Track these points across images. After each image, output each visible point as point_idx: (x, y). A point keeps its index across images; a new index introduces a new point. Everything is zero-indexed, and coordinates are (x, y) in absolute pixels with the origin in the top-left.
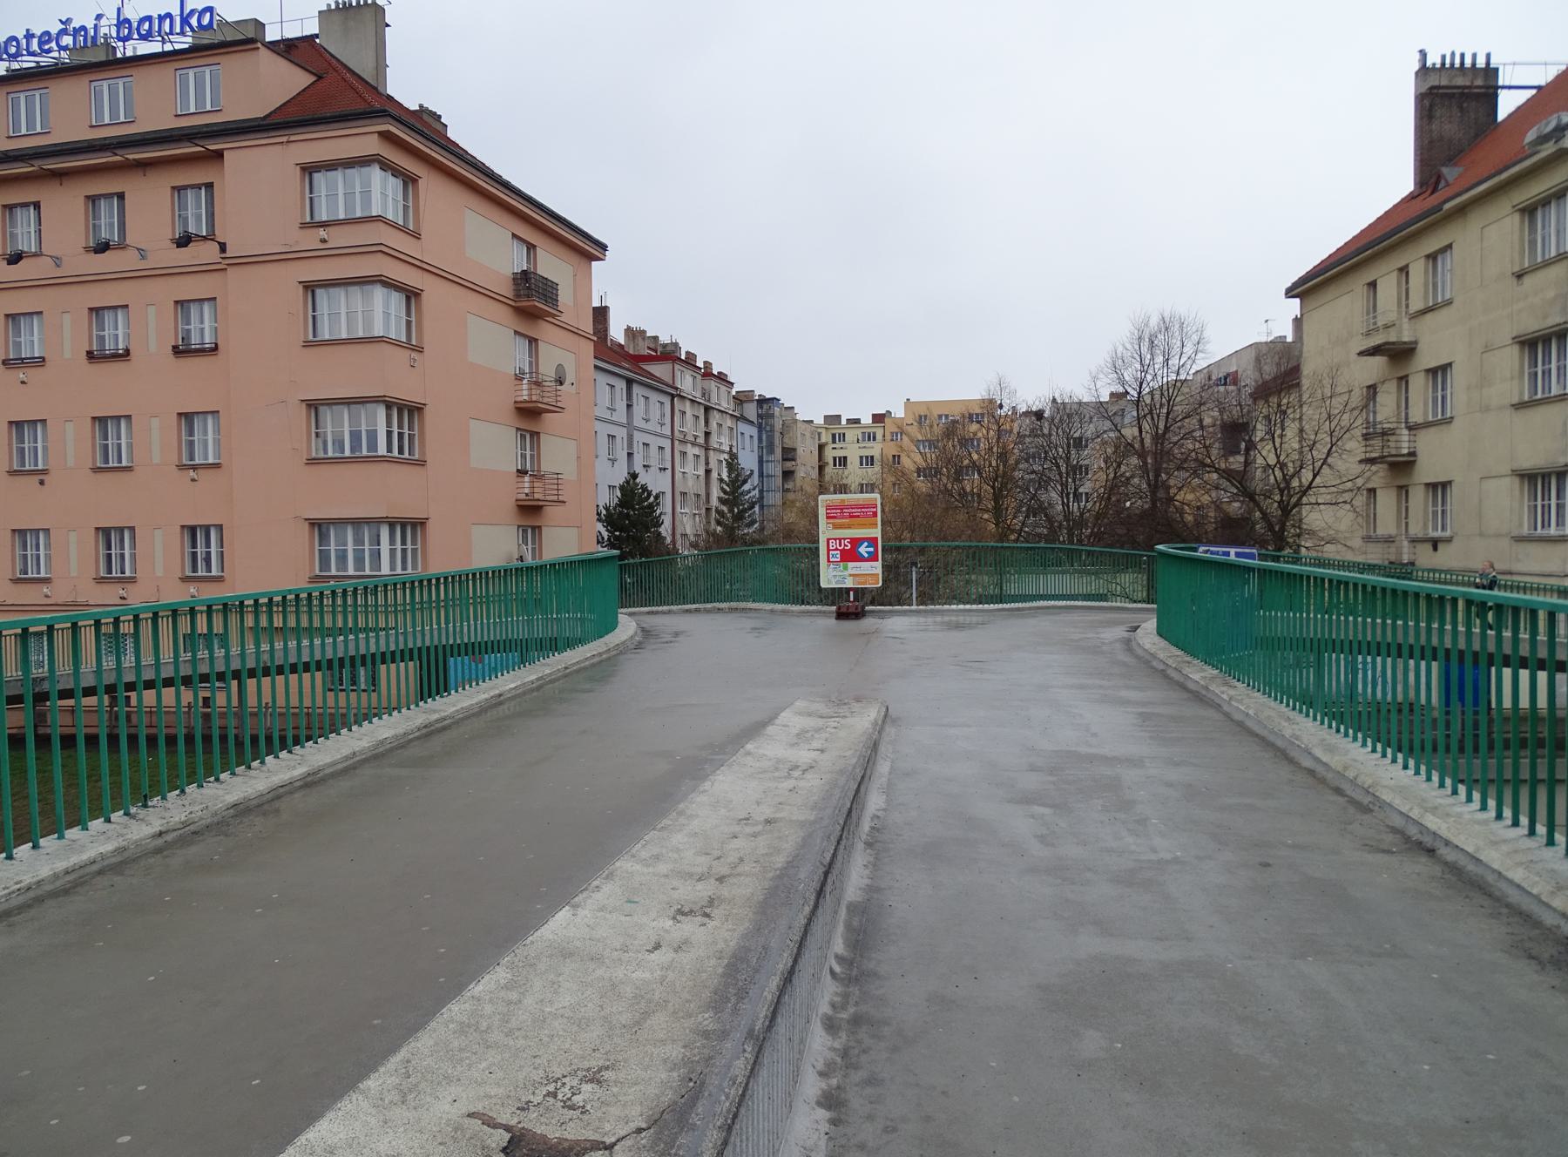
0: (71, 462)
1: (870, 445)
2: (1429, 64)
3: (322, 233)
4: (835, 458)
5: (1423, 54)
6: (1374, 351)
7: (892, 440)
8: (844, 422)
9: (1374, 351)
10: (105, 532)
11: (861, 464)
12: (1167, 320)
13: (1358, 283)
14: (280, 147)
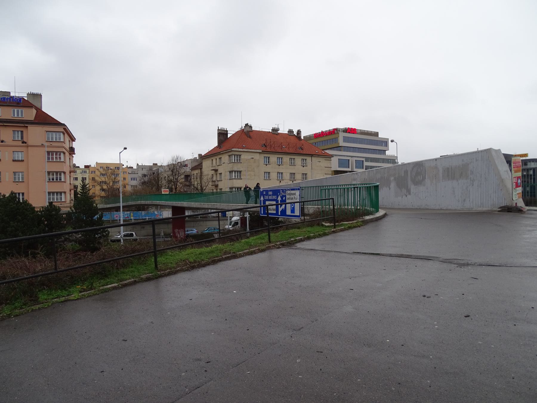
0: (7, 180)
3: (51, 143)
5: (218, 127)
6: (213, 170)
7: (92, 173)
9: (213, 170)
12: (178, 156)
13: (211, 159)
14: (42, 127)
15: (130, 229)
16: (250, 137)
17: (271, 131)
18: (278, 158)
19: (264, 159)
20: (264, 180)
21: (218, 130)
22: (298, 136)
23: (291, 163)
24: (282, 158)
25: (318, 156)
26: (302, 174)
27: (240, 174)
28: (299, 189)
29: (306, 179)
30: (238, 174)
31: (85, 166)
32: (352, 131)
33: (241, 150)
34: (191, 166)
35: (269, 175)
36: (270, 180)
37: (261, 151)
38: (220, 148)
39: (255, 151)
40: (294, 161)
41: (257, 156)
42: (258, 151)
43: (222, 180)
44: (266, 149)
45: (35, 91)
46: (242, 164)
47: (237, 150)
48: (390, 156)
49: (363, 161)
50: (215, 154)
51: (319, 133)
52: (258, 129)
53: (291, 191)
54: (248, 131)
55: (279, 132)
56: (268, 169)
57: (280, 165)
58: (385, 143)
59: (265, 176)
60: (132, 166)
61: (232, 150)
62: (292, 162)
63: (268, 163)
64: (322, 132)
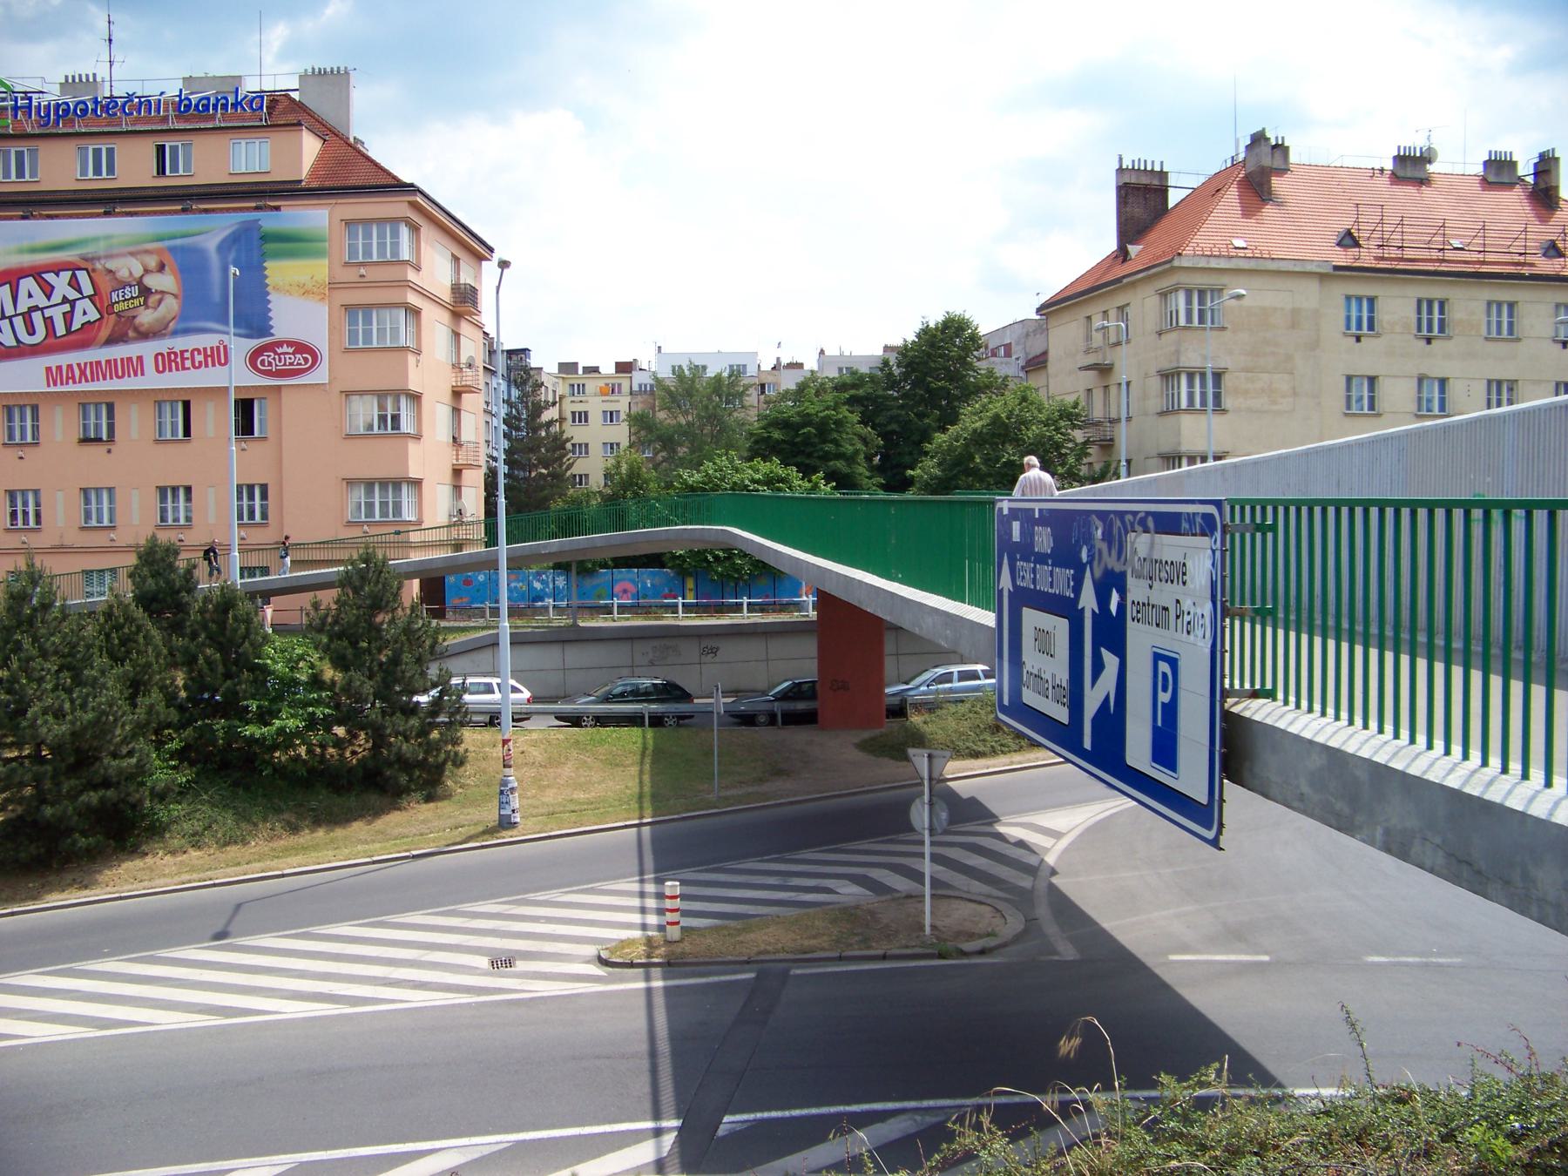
1: (616, 398)
2: (1124, 167)
3: (362, 271)
4: (573, 413)
5: (1121, 159)
6: (1088, 368)
8: (580, 371)
9: (1088, 368)
10: (85, 491)
11: (605, 421)
15: (651, 656)
19: (1349, 309)
21: (1120, 171)
22: (1542, 186)
26: (1489, 382)
28: (1207, 526)
31: (617, 364)
34: (1027, 354)
46: (1227, 333)
53: (1158, 536)
56: (1368, 357)
57: (1435, 338)
60: (800, 361)
62: (1499, 324)
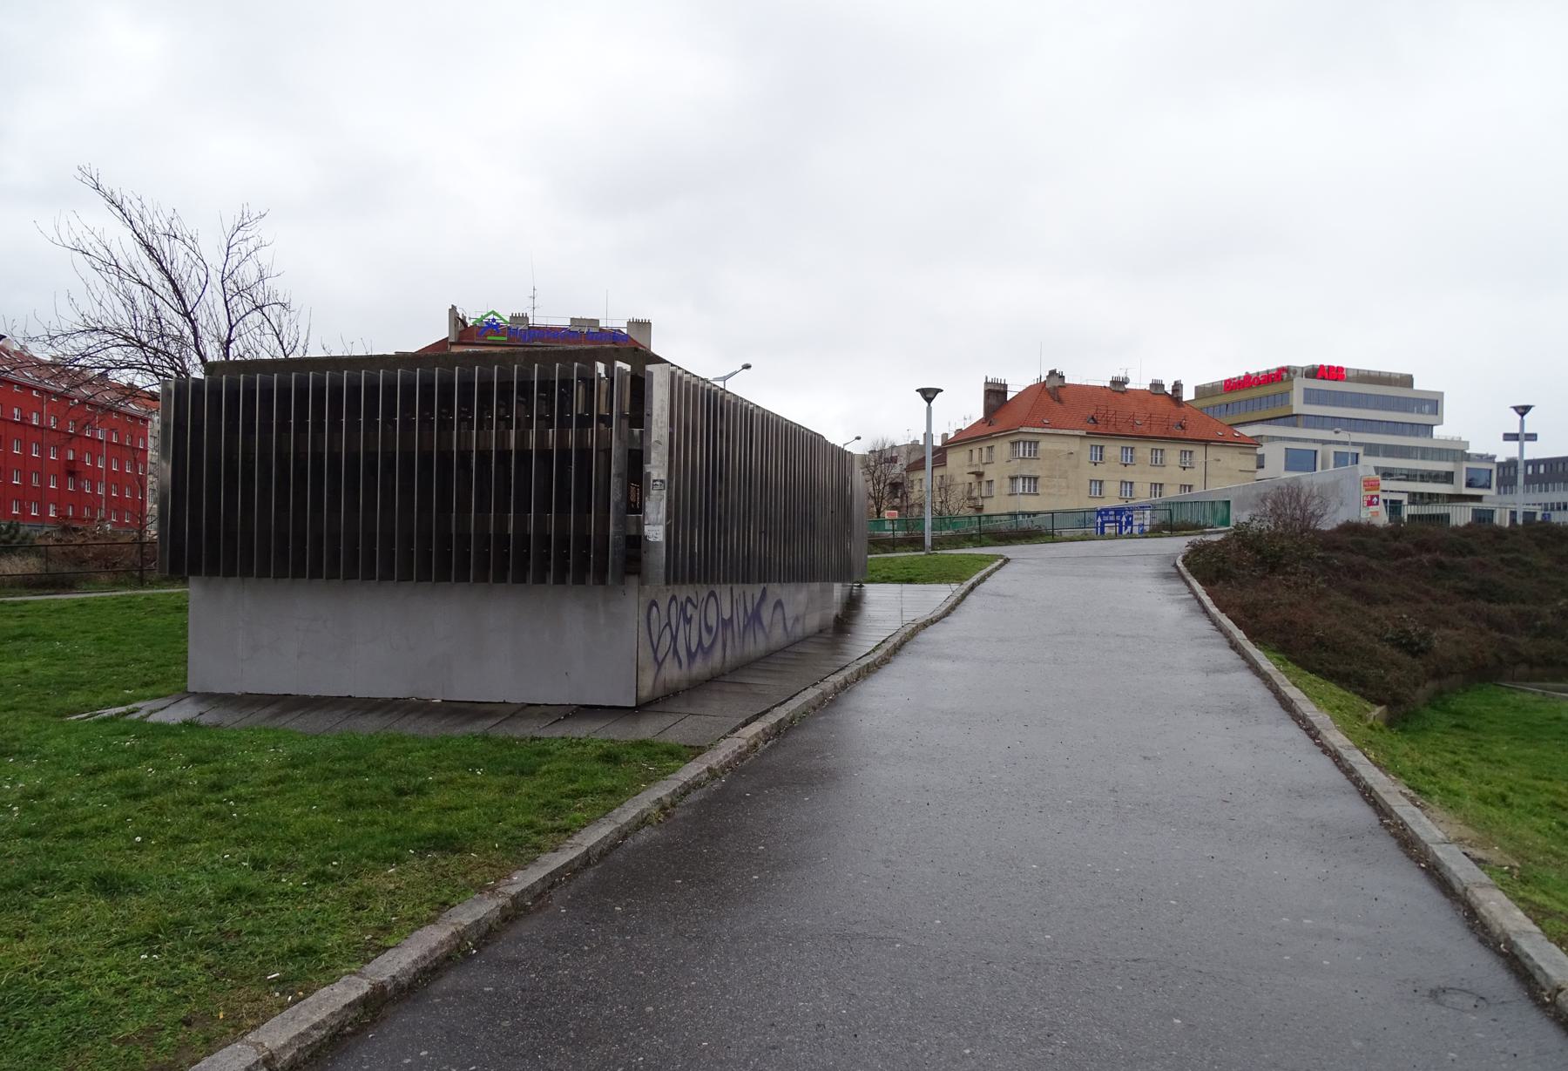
5: (987, 378)
6: (973, 473)
9: (973, 473)
16: (1060, 401)
17: (1108, 385)
18: (1122, 448)
20: (1090, 497)
21: (987, 383)
22: (1175, 396)
23: (1154, 462)
24: (1132, 449)
25: (1223, 443)
26: (1181, 485)
27: (1035, 482)
29: (1160, 496)
30: (1030, 483)
32: (1334, 373)
33: (1040, 430)
35: (1100, 486)
36: (1103, 497)
37: (1084, 433)
38: (989, 425)
39: (1071, 432)
40: (1161, 455)
41: (1075, 445)
42: (1077, 432)
43: (992, 497)
44: (1096, 428)
45: (641, 317)
47: (1031, 430)
48: (1446, 440)
49: (1357, 454)
50: (971, 439)
51: (1239, 377)
52: (1077, 382)
54: (1055, 388)
55: (1127, 386)
56: (1099, 473)
58: (1433, 404)
59: (1090, 490)
61: (1021, 430)
62: (1156, 458)
63: (1098, 460)
64: (1248, 376)
